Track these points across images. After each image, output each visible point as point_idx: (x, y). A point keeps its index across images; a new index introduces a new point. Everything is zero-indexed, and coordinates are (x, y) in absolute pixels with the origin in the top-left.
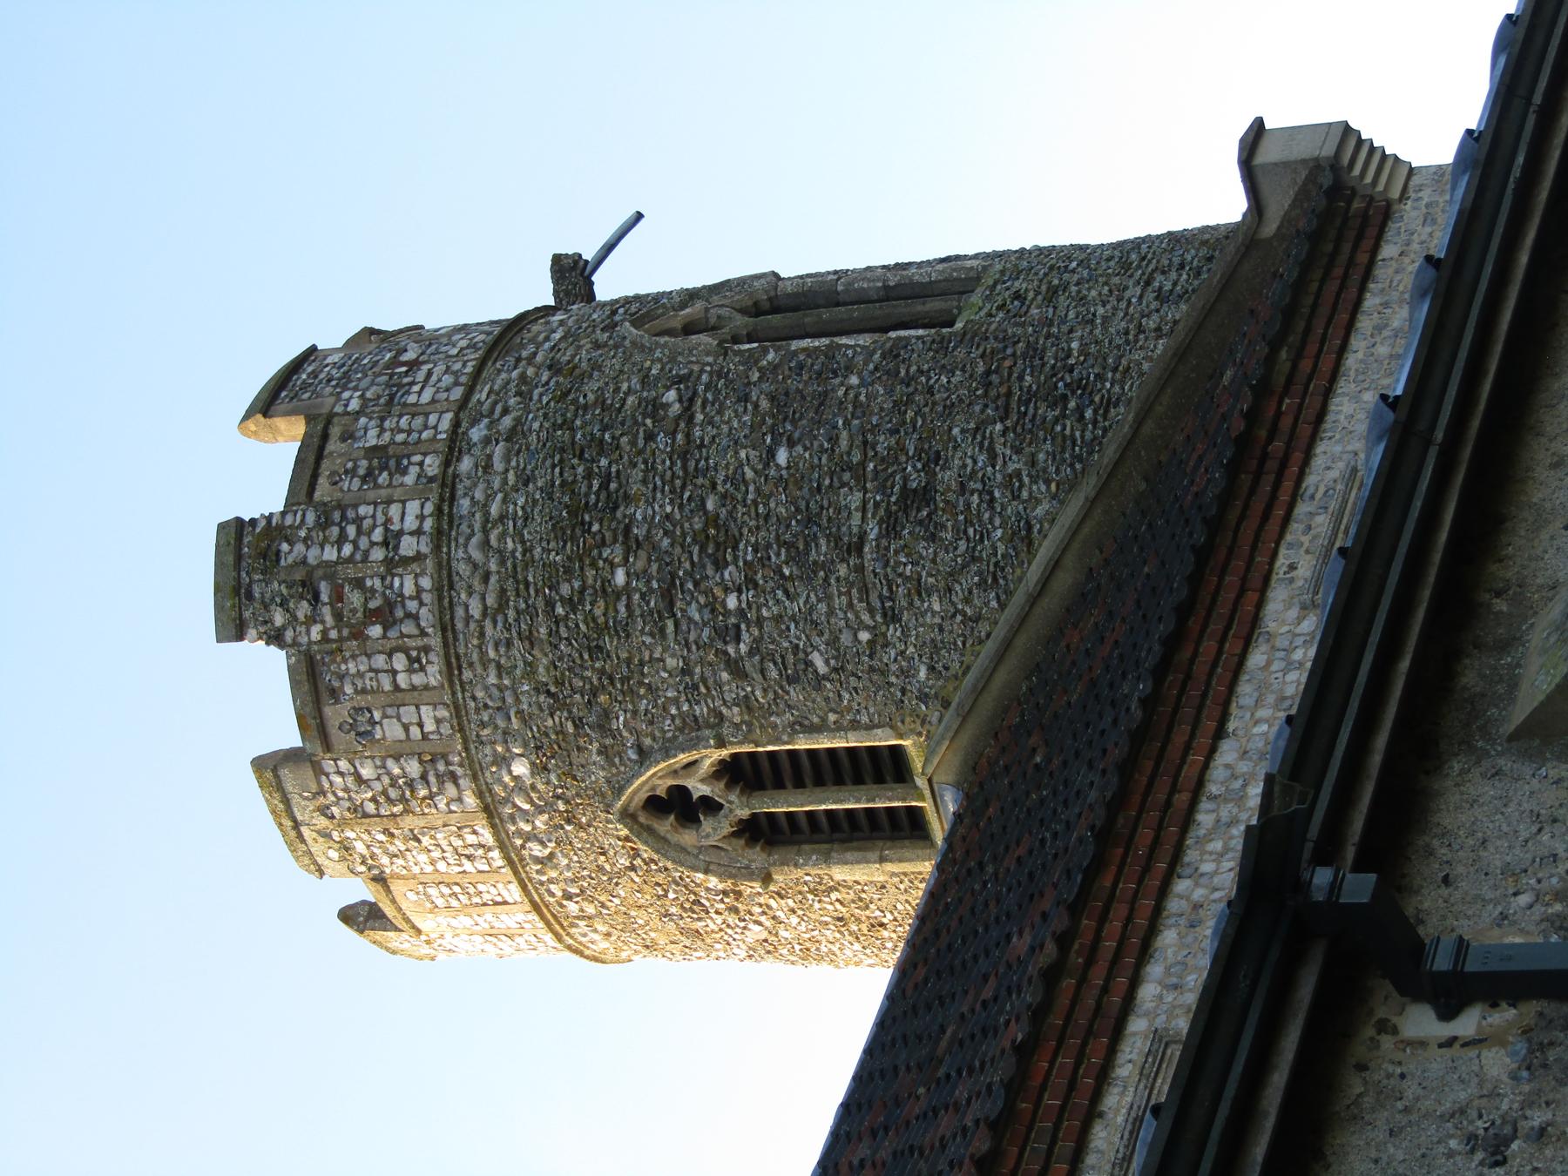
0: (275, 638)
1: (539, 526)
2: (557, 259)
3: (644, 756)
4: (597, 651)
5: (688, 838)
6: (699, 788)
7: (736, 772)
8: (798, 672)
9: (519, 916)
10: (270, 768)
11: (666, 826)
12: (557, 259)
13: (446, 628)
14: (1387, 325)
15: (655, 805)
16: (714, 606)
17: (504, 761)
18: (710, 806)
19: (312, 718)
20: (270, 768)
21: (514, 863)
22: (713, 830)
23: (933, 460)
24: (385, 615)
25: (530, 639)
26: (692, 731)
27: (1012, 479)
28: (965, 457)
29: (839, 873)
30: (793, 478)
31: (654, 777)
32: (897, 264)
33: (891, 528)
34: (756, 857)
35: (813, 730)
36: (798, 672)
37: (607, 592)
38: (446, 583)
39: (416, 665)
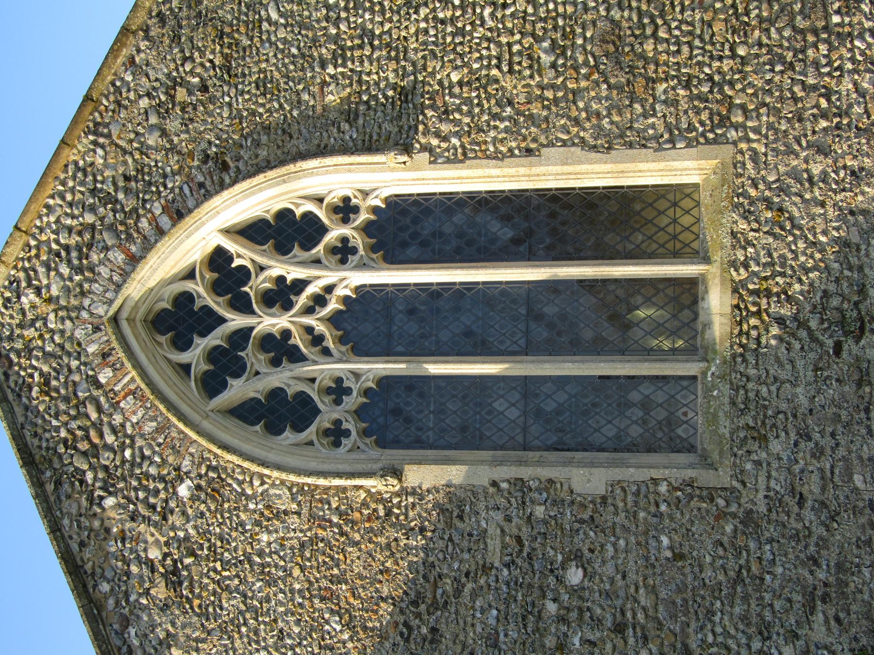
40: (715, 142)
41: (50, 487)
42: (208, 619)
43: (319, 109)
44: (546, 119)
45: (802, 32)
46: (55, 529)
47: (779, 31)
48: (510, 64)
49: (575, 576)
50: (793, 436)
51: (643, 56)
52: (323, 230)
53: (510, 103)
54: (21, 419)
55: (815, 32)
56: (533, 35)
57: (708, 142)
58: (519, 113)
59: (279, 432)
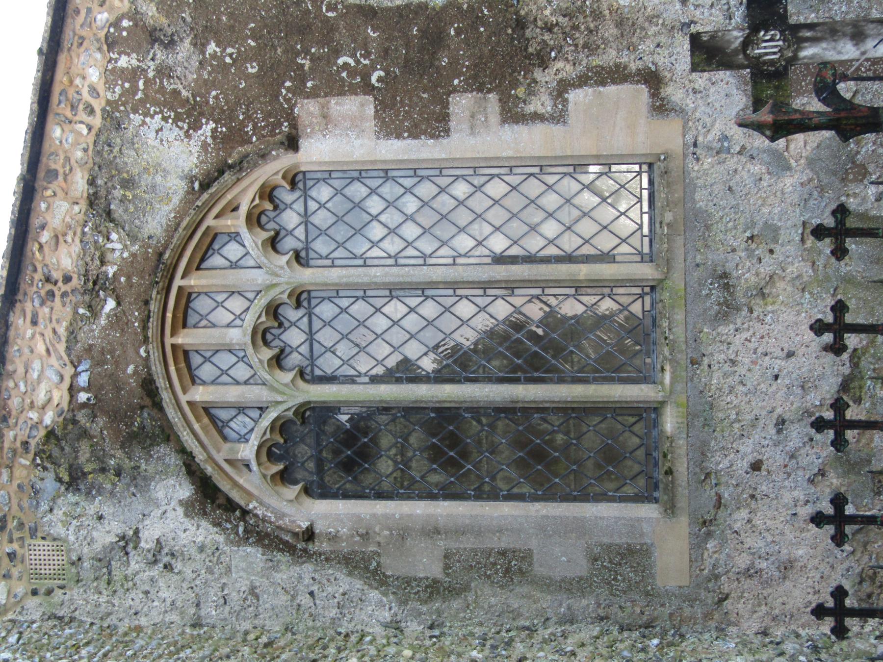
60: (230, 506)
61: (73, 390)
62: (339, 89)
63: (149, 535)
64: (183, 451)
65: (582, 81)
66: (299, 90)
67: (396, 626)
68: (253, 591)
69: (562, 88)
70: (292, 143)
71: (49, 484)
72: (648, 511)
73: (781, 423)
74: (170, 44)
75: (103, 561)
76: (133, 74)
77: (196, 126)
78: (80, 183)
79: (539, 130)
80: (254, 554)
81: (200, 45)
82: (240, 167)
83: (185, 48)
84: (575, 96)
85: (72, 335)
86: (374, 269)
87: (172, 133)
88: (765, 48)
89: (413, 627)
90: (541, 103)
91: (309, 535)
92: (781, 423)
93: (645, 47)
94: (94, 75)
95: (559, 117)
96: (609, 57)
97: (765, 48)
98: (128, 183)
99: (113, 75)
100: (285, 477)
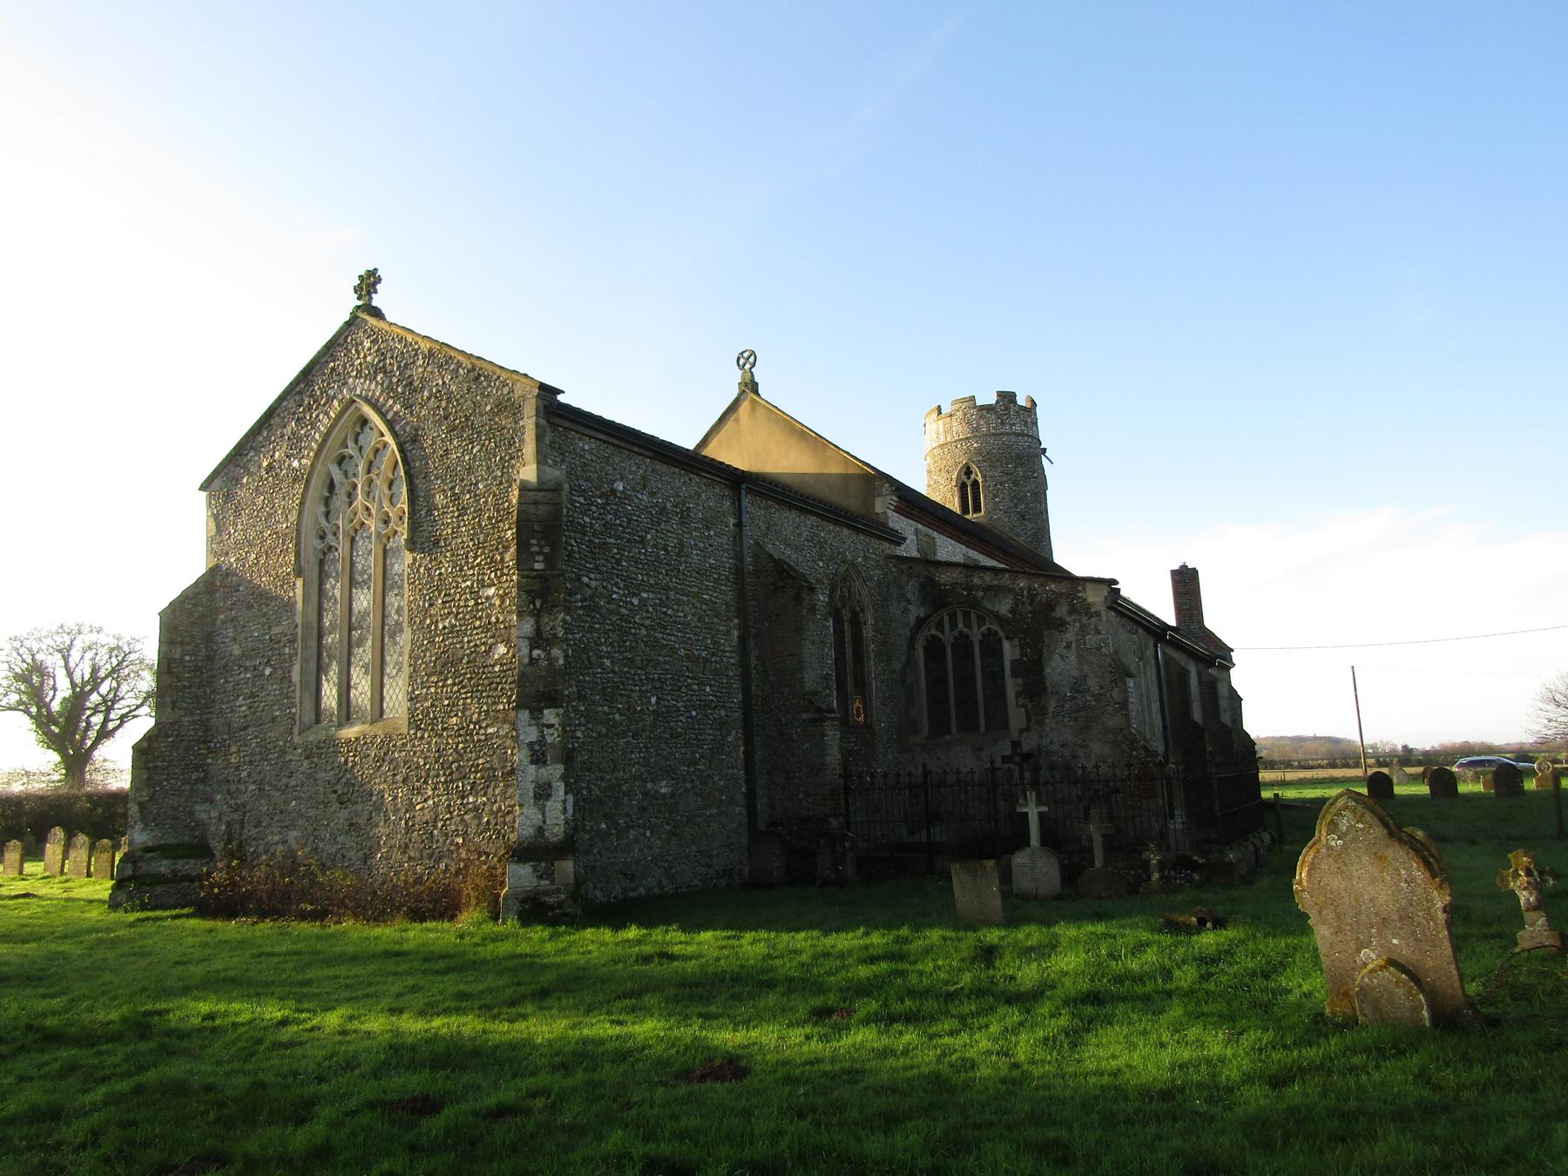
0: (997, 402)
1: (1017, 451)
2: (1174, 573)
3: (979, 468)
4: (997, 461)
5: (963, 473)
6: (973, 476)
7: (975, 483)
8: (995, 496)
9: (942, 440)
10: (973, 399)
11: (965, 469)
12: (1174, 573)
13: (1001, 434)
14: (143, 818)
15: (968, 468)
16: (1006, 482)
17: (976, 442)
18: (969, 478)
19: (983, 408)
20: (973, 399)
21: (955, 441)
22: (964, 478)
23: (1029, 520)
24: (1002, 423)
25: (999, 449)
26: (984, 476)
27: (1026, 533)
28: (1030, 526)
29: (957, 499)
30: (1026, 496)
31: (974, 468)
32: (757, 384)
33: (1018, 513)
34: (959, 485)
35: (985, 498)
36: (995, 496)
37: (1007, 464)
38: (1008, 434)
39: (994, 428)
40: (410, 723)
41: (297, 389)
42: (696, 1146)
43: (432, 492)
44: (423, 627)
45: (450, 767)
46: (282, 398)
47: (451, 754)
48: (446, 602)
49: (268, 671)
50: (309, 771)
51: (446, 679)
52: (961, 633)
53: (431, 605)
54: (322, 361)
55: (451, 774)
56: (458, 613)
57: (409, 719)
58: (426, 610)
59: (1310, 928)
60: (920, 627)
61: (944, 585)
62: (1022, 649)
63: (912, 607)
64: (931, 615)
65: (1026, 711)
66: (1021, 639)
67: (894, 672)
68: (899, 635)
69: (1024, 706)
70: (1007, 638)
71: (921, 580)
72: (926, 733)
73: (949, 764)
74: (1031, 604)
75: (904, 596)
76: (1022, 595)
77: (1011, 612)
78: (995, 583)
79: (1014, 701)
80: (909, 634)
81: (1030, 612)
82: (1001, 626)
83: (1030, 608)
84: (1023, 710)
85: (957, 583)
86: (1152, 648)
87: (1008, 606)
88: (1334, 781)
89: (895, 676)
90: (1021, 701)
91: (914, 649)
92: (949, 764)
93: (1036, 726)
94: (1022, 584)
95: (1017, 705)
96: (1033, 718)
97: (1334, 781)
98: (995, 596)
99: (1022, 589)
100: (927, 641)
